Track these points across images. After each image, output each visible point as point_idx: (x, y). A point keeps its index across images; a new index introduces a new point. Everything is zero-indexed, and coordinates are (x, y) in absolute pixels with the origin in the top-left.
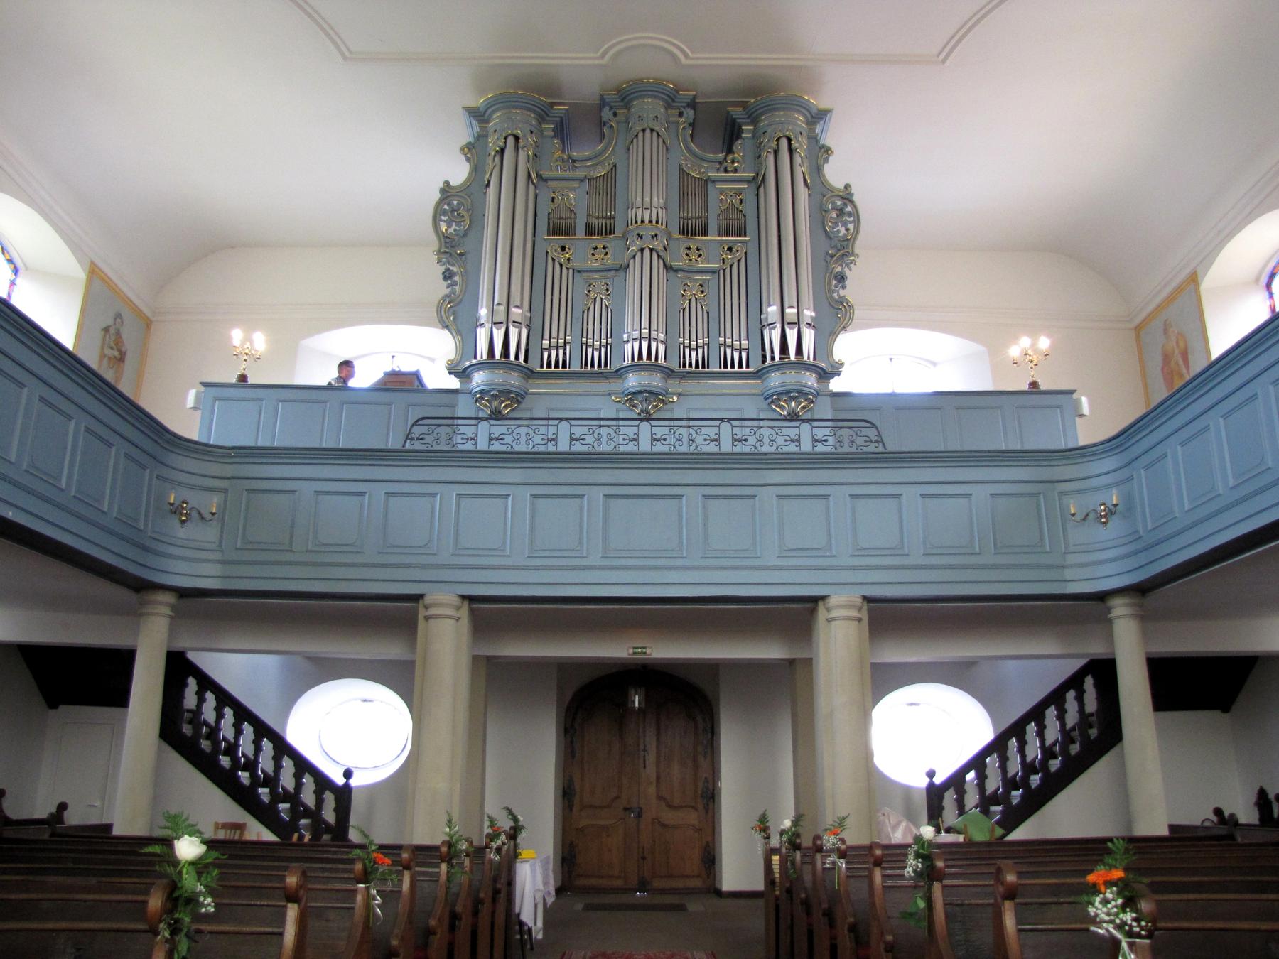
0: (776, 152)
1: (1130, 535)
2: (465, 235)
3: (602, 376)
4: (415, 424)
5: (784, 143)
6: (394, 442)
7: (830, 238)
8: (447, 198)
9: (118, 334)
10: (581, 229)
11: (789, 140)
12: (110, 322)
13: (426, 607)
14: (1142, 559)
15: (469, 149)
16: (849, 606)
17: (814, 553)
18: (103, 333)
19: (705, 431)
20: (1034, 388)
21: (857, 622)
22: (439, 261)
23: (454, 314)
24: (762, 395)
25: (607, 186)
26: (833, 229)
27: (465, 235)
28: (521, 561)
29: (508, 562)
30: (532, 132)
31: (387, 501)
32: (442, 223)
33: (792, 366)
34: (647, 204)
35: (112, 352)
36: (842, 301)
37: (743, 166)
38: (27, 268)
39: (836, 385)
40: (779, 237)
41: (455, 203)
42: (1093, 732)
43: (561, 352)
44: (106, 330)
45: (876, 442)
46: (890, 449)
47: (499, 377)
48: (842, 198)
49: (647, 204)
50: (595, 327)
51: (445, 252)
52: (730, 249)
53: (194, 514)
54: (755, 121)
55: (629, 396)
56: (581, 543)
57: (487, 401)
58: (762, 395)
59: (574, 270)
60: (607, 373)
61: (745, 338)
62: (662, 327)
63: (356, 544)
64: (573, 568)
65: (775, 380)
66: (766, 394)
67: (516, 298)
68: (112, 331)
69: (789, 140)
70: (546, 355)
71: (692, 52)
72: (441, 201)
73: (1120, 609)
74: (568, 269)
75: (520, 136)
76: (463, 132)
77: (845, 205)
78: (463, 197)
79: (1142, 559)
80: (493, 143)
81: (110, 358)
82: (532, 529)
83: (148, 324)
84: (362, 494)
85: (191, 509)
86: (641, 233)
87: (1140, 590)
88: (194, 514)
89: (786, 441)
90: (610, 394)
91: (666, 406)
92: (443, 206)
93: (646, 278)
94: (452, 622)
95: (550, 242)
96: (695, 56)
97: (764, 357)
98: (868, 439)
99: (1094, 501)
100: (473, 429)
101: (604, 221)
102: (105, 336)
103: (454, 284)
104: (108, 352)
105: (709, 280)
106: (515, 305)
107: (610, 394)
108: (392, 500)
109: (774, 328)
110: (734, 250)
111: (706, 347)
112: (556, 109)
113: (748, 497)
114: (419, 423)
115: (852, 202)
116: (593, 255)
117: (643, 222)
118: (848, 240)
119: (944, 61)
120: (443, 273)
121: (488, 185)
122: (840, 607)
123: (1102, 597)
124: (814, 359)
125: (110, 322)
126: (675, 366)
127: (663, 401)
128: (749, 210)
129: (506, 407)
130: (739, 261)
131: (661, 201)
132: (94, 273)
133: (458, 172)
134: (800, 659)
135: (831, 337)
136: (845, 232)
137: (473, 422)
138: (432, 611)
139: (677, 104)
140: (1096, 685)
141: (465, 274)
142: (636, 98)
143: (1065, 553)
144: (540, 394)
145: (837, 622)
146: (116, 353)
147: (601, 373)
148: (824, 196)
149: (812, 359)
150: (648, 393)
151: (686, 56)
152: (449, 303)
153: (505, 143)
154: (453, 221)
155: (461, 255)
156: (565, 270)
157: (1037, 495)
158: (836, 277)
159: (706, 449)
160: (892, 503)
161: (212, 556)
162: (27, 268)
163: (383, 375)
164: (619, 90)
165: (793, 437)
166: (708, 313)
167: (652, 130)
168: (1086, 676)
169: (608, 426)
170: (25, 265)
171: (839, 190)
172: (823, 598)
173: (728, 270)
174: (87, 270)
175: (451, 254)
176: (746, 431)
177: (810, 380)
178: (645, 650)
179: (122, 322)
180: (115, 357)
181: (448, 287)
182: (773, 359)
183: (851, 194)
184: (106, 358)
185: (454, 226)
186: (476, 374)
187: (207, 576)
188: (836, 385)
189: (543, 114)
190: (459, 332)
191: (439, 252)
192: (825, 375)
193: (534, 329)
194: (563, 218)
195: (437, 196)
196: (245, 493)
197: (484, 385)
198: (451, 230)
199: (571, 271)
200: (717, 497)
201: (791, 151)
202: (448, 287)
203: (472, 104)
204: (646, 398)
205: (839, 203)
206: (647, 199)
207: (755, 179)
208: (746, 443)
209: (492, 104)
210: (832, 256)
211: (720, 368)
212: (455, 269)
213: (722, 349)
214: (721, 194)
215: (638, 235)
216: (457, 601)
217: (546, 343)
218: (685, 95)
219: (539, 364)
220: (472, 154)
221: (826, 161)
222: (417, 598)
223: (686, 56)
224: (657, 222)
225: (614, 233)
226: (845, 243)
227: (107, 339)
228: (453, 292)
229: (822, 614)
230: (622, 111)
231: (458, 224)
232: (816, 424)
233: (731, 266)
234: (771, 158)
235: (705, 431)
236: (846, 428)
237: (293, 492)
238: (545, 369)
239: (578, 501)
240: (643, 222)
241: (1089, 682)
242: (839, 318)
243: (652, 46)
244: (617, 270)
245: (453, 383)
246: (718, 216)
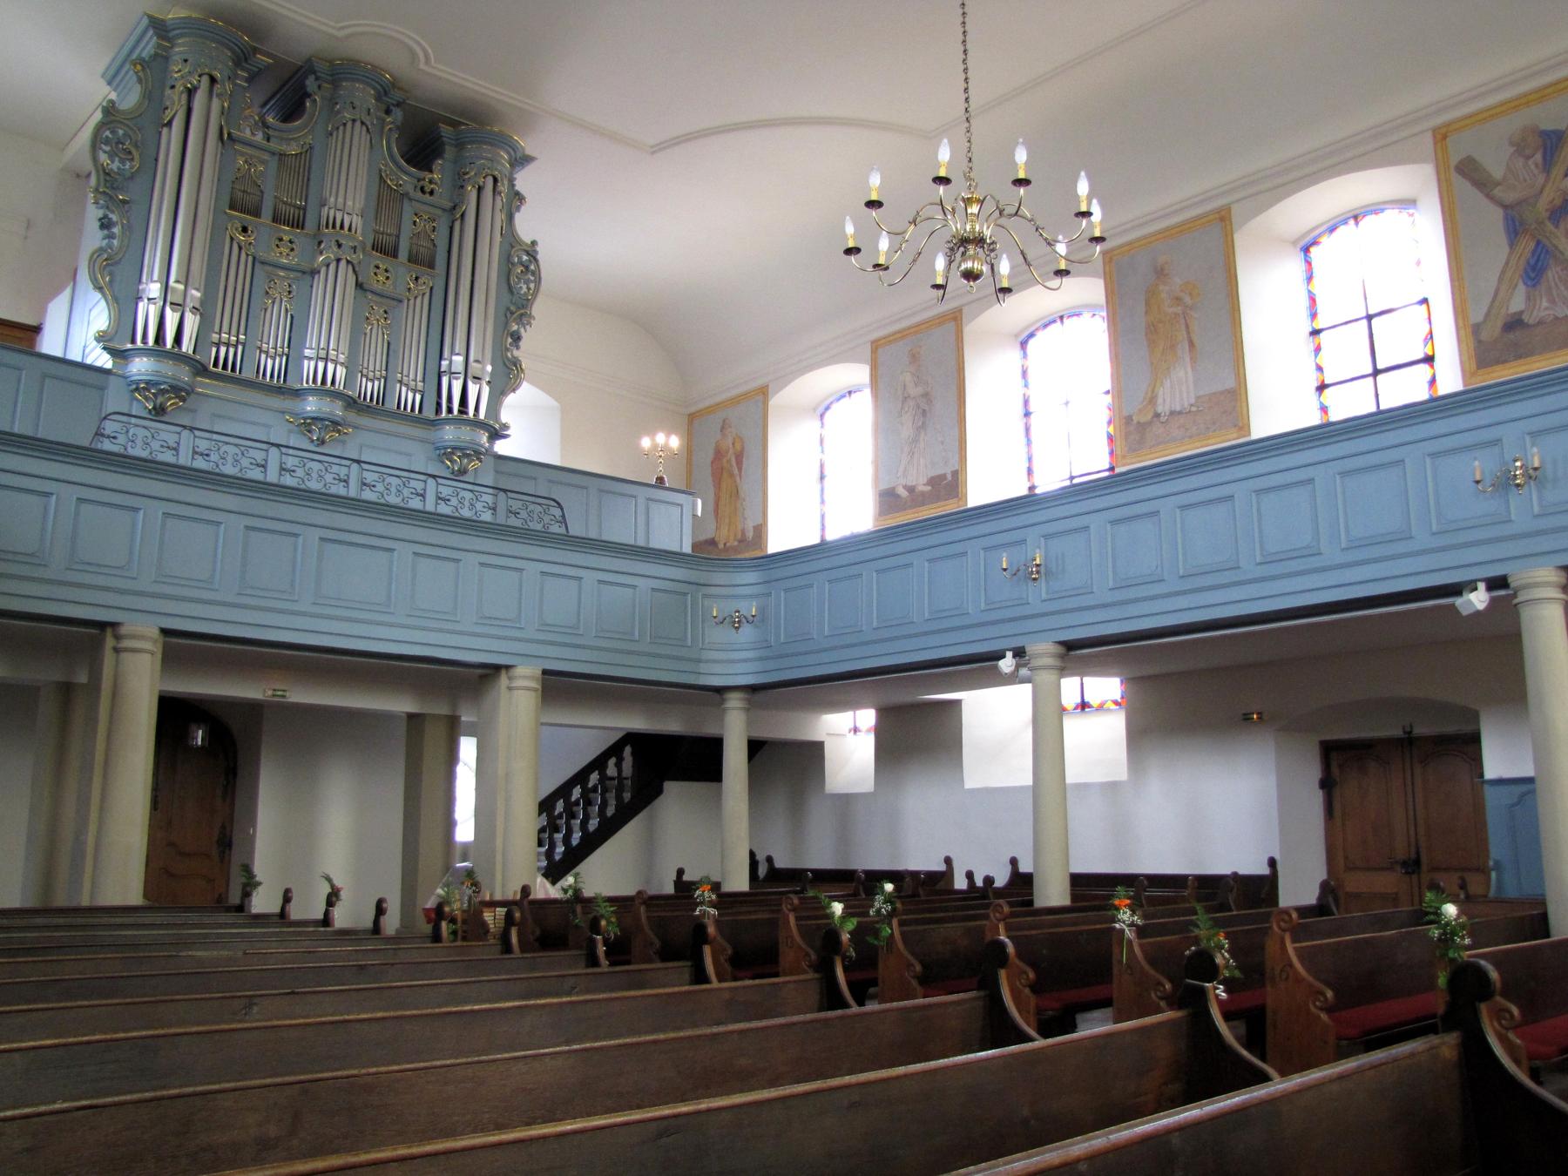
0: (480, 189)
1: (752, 643)
2: (132, 178)
3: (280, 391)
5: (490, 180)
8: (111, 122)
10: (403, 254)
14: (771, 665)
19: (252, 453)
20: (661, 483)
23: (111, 274)
24: (433, 444)
25: (300, 168)
27: (132, 178)
28: (231, 598)
32: (101, 153)
34: (340, 206)
36: (516, 363)
37: (440, 190)
39: (501, 447)
40: (472, 282)
41: (121, 132)
42: (627, 796)
43: (232, 350)
46: (571, 533)
47: (169, 369)
48: (528, 254)
49: (348, 209)
50: (274, 332)
51: (104, 193)
54: (460, 145)
55: (308, 421)
56: (292, 586)
57: (153, 394)
58: (433, 444)
59: (254, 258)
60: (285, 390)
61: (227, 331)
62: (344, 347)
63: (37, 554)
65: (449, 434)
69: (495, 180)
71: (435, 62)
73: (735, 702)
74: (247, 255)
75: (219, 80)
77: (530, 261)
78: (131, 129)
79: (771, 665)
84: (47, 495)
86: (341, 241)
87: (753, 689)
89: (162, 446)
90: (283, 413)
92: (104, 132)
93: (461, 331)
94: (150, 655)
95: (231, 218)
96: (435, 65)
97: (439, 405)
98: (165, 444)
99: (730, 607)
100: (263, 454)
103: (111, 236)
107: (283, 413)
108: (84, 507)
109: (457, 379)
111: (240, 348)
112: (259, 59)
113: (516, 569)
115: (536, 260)
118: (528, 300)
119: (653, 153)
122: (525, 677)
123: (720, 691)
124: (344, 388)
127: (339, 432)
128: (442, 241)
130: (424, 294)
134: (429, 714)
136: (526, 290)
137: (264, 446)
138: (126, 643)
139: (388, 100)
140: (633, 754)
141: (127, 229)
142: (346, 79)
143: (702, 649)
144: (207, 396)
145: (520, 691)
147: (280, 388)
149: (342, 388)
150: (331, 422)
152: (106, 260)
154: (117, 155)
155: (124, 202)
157: (685, 594)
159: (161, 457)
160: (574, 584)
165: (259, 461)
166: (389, 344)
168: (626, 745)
169: (319, 461)
171: (527, 244)
172: (508, 667)
173: (412, 302)
177: (484, 438)
178: (285, 694)
181: (104, 239)
182: (450, 410)
183: (536, 252)
186: (137, 360)
188: (501, 447)
189: (242, 58)
190: (116, 299)
192: (497, 434)
194: (247, 192)
197: (148, 375)
199: (250, 258)
202: (104, 239)
205: (525, 258)
206: (340, 200)
209: (187, 25)
210: (512, 313)
212: (114, 217)
215: (337, 241)
216: (155, 633)
218: (397, 95)
219: (130, 338)
221: (518, 209)
224: (350, 229)
225: (303, 228)
229: (503, 680)
231: (122, 161)
232: (366, 466)
233: (416, 298)
235: (163, 436)
236: (232, 444)
238: (220, 370)
240: (342, 227)
241: (628, 750)
244: (304, 273)
245: (105, 361)
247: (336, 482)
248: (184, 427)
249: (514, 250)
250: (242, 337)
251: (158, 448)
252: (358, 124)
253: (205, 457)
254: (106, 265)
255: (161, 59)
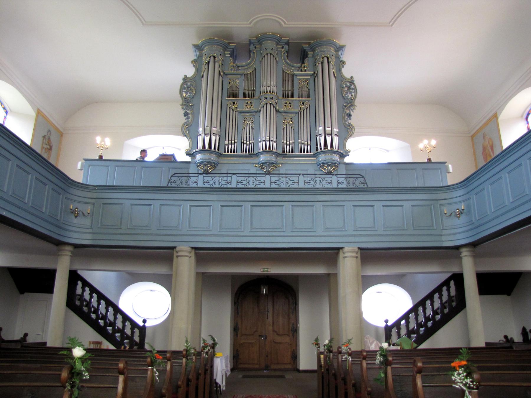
0: (322, 63)
1: (469, 222)
2: (193, 97)
3: (250, 156)
4: (172, 176)
5: (326, 59)
6: (164, 184)
7: (345, 99)
8: (185, 82)
9: (49, 138)
11: (328, 58)
12: (46, 134)
13: (177, 252)
14: (474, 232)
15: (195, 62)
16: (353, 252)
17: (338, 230)
18: (43, 138)
19: (293, 179)
20: (429, 161)
21: (356, 258)
22: (182, 108)
23: (189, 130)
24: (317, 164)
25: (252, 77)
26: (346, 95)
27: (193, 97)
28: (216, 233)
29: (211, 233)
30: (221, 55)
31: (160, 208)
32: (183, 93)
33: (329, 152)
34: (269, 85)
35: (47, 146)
36: (350, 125)
37: (308, 69)
38: (11, 111)
39: (347, 160)
40: (324, 98)
41: (189, 84)
43: (233, 146)
44: (44, 137)
45: (364, 183)
46: (369, 186)
47: (207, 156)
48: (350, 82)
49: (269, 85)
50: (247, 136)
51: (185, 105)
52: (303, 103)
53: (81, 213)
54: (313, 50)
55: (261, 165)
56: (241, 225)
57: (202, 166)
58: (317, 164)
59: (238, 112)
60: (252, 155)
61: (309, 140)
62: (275, 136)
63: (148, 226)
64: (238, 236)
65: (322, 158)
66: (318, 163)
67: (214, 124)
68: (47, 137)
69: (328, 58)
70: (227, 147)
71: (287, 22)
72: (183, 84)
73: (465, 253)
74: (236, 112)
75: (216, 56)
76: (192, 55)
77: (351, 85)
78: (192, 82)
79: (474, 232)
80: (205, 59)
81: (46, 149)
82: (221, 220)
83: (61, 134)
84: (150, 205)
85: (79, 211)
86: (266, 97)
87: (473, 245)
88: (81, 213)
89: (326, 183)
91: (277, 169)
93: (268, 115)
94: (188, 258)
95: (228, 100)
96: (288, 23)
97: (317, 148)
98: (360, 182)
99: (454, 208)
100: (196, 178)
101: (251, 92)
102: (43, 139)
103: (189, 118)
104: (45, 146)
105: (294, 116)
106: (214, 126)
107: (253, 164)
108: (163, 207)
109: (321, 136)
110: (305, 104)
111: (293, 144)
112: (231, 45)
113: (311, 206)
114: (174, 175)
115: (354, 84)
116: (246, 106)
117: (267, 92)
118: (352, 99)
119: (392, 25)
120: (184, 113)
121: (203, 77)
122: (349, 252)
123: (457, 248)
125: (46, 134)
126: (280, 152)
127: (275, 167)
128: (311, 87)
129: (210, 169)
130: (307, 108)
131: (274, 83)
132: (39, 113)
133: (190, 72)
135: (345, 140)
136: (351, 96)
137: (196, 175)
138: (180, 254)
141: (193, 114)
143: (442, 229)
144: (224, 163)
145: (348, 258)
146: (48, 147)
147: (250, 155)
148: (342, 82)
150: (269, 163)
151: (285, 23)
152: (187, 126)
153: (210, 59)
154: (188, 92)
155: (192, 106)
156: (234, 112)
157: (431, 205)
158: (347, 115)
159: (293, 186)
160: (370, 209)
161: (88, 231)
162: (11, 111)
163: (159, 156)
164: (257, 37)
165: (329, 181)
166: (294, 130)
167: (271, 54)
169: (253, 177)
170: (10, 110)
171: (348, 79)
172: (342, 248)
173: (302, 112)
174: (36, 112)
175: (187, 106)
176: (310, 179)
177: (336, 158)
179: (51, 134)
180: (48, 148)
181: (186, 119)
182: (321, 149)
183: (353, 81)
184: (44, 149)
185: (188, 94)
186: (197, 155)
187: (86, 239)
188: (347, 160)
189: (225, 48)
190: (190, 138)
191: (182, 105)
192: (343, 155)
193: (222, 137)
194: (234, 91)
195: (182, 81)
196: (102, 205)
197: (201, 160)
198: (187, 96)
199: (237, 112)
200: (298, 206)
201: (328, 63)
202: (186, 119)
203: (196, 43)
204: (268, 165)
205: (348, 84)
206: (269, 83)
207: (313, 74)
208: (310, 184)
209: (204, 43)
210: (346, 106)
211: (299, 153)
212: (189, 112)
213: (300, 145)
214: (300, 80)
215: (265, 97)
216: (190, 249)
217: (227, 142)
218: (285, 40)
219: (224, 151)
220: (196, 64)
221: (343, 67)
222: (173, 248)
223: (285, 23)
224: (273, 92)
225: (255, 97)
226: (351, 101)
227: (45, 141)
228: (188, 121)
230: (258, 46)
231: (190, 93)
232: (339, 176)
233: (304, 110)
234: (320, 65)
235: (293, 179)
236: (351, 177)
237: (122, 204)
238: (226, 153)
239: (240, 208)
240: (267, 92)
242: (348, 132)
243: (271, 19)
244: (256, 112)
245: (188, 159)
246: (298, 90)
247: (226, 184)
248: (300, 174)
249: (342, 82)
250: (253, 141)
251: (258, 183)
252: (269, 54)
253: (342, 184)
254: (187, 127)
255: (200, 57)
